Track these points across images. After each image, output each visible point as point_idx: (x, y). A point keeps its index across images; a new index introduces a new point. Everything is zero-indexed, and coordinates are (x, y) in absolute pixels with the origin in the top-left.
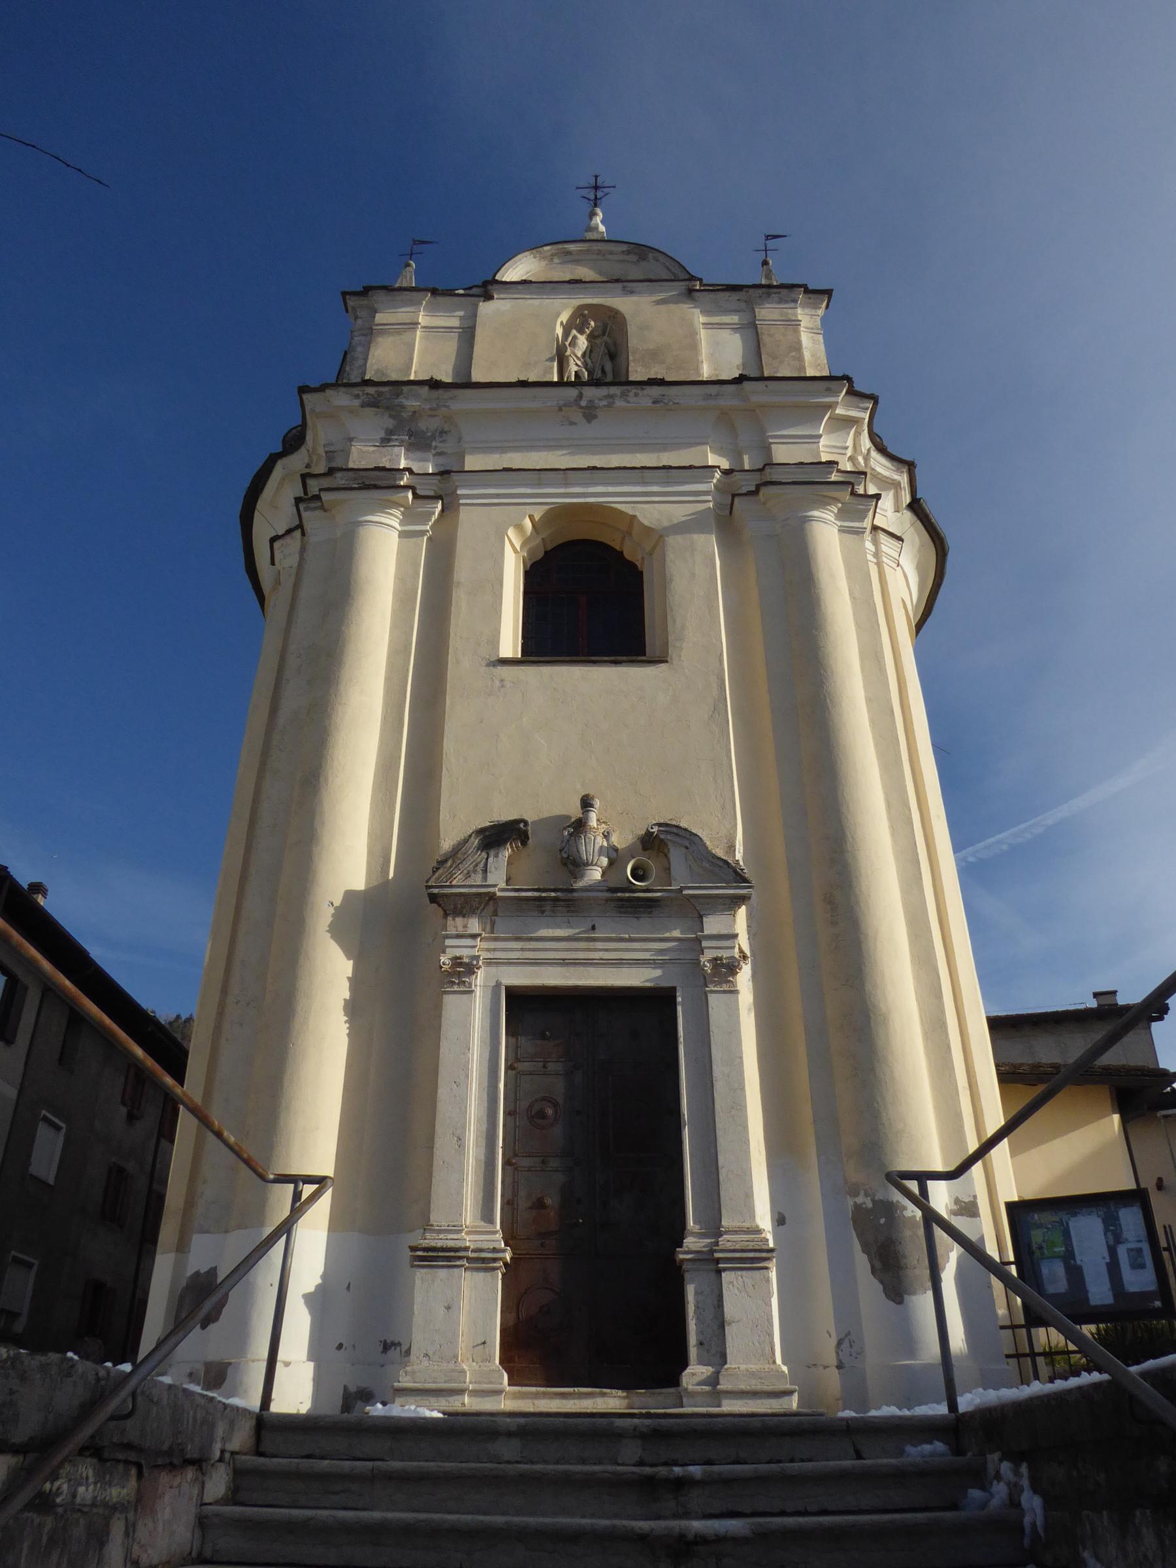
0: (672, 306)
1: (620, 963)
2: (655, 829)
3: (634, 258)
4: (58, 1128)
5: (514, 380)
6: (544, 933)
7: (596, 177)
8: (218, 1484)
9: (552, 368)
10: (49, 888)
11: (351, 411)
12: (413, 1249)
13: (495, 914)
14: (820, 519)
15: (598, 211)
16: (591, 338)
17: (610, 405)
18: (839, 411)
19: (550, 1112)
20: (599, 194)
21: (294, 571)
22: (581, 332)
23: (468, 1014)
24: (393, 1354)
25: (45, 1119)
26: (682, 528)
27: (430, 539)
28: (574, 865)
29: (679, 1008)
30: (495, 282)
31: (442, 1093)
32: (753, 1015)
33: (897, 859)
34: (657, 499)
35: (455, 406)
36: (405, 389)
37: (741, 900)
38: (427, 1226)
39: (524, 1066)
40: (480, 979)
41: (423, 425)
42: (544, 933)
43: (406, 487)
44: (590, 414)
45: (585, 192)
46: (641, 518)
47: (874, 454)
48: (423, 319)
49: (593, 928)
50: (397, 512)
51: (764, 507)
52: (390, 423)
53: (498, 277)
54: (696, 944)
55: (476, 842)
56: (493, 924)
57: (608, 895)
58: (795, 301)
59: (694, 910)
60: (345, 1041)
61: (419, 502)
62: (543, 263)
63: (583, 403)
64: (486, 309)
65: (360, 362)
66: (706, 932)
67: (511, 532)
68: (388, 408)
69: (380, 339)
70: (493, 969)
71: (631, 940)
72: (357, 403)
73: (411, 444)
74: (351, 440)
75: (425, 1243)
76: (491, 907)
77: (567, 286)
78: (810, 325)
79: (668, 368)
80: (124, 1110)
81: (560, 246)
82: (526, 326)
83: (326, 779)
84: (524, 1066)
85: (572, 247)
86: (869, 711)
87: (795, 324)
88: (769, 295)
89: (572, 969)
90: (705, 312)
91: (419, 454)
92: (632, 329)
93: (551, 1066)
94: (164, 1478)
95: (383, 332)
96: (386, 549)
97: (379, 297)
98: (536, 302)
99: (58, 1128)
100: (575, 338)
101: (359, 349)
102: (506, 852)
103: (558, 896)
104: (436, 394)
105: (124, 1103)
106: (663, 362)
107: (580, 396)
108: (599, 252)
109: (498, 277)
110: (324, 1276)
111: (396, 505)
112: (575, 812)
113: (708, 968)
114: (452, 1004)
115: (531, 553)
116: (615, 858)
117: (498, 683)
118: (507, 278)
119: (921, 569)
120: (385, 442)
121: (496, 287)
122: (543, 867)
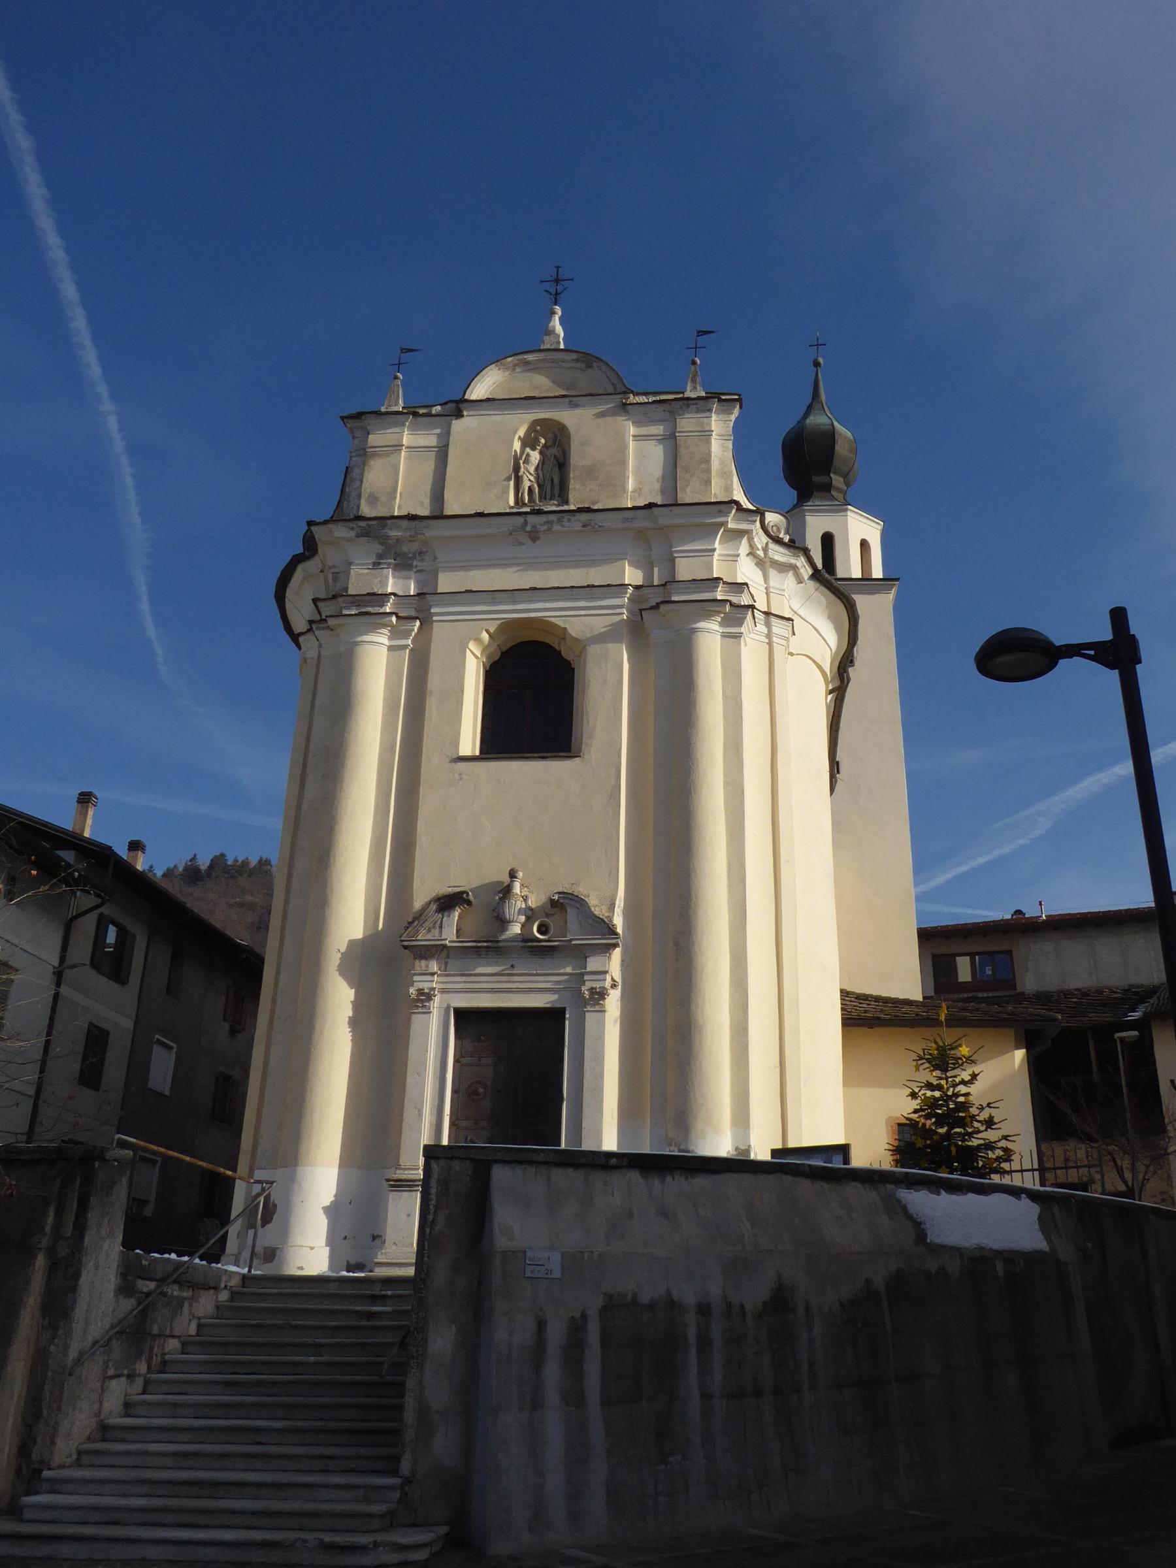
0: (609, 419)
1: (528, 991)
2: (556, 897)
3: (580, 365)
4: (170, 1048)
5: (473, 512)
6: (480, 970)
7: (558, 268)
8: (224, 1296)
9: (508, 487)
10: (146, 843)
11: (349, 540)
12: (388, 1180)
13: (448, 956)
14: (708, 631)
15: (558, 309)
16: (541, 453)
17: (549, 529)
18: (730, 526)
19: (481, 1090)
20: (560, 288)
21: (315, 662)
22: (533, 449)
23: (427, 1028)
24: (378, 1241)
25: (159, 1042)
26: (602, 638)
27: (411, 650)
28: (503, 922)
29: (567, 1022)
30: (463, 401)
31: (409, 1080)
32: (618, 1025)
33: (730, 909)
34: (583, 612)
35: (429, 533)
36: (389, 522)
37: (615, 946)
38: (398, 1166)
39: (464, 1060)
40: (436, 1004)
41: (405, 548)
42: (480, 970)
43: (391, 614)
44: (534, 536)
45: (546, 286)
46: (570, 631)
47: (772, 546)
48: (406, 439)
49: (512, 966)
50: (385, 631)
51: (666, 619)
52: (379, 548)
53: (466, 397)
54: (580, 978)
55: (434, 907)
56: (446, 964)
57: (521, 944)
58: (710, 410)
59: (581, 953)
60: (350, 1044)
61: (403, 622)
62: (507, 373)
63: (528, 528)
64: (458, 426)
65: (357, 484)
66: (588, 969)
67: (472, 645)
68: (376, 538)
69: (372, 462)
70: (445, 995)
71: (537, 975)
72: (352, 534)
73: (396, 565)
74: (350, 564)
75: (395, 1177)
76: (445, 953)
77: (525, 402)
78: (723, 432)
79: (601, 485)
80: (227, 1026)
81: (521, 357)
82: (486, 453)
83: (334, 858)
84: (464, 1060)
85: (530, 357)
86: (725, 793)
87: (706, 434)
88: (688, 406)
89: (497, 995)
90: (637, 424)
91: (404, 573)
92: (574, 446)
93: (484, 1061)
94: (202, 1292)
95: (375, 455)
96: (377, 661)
97: (371, 421)
98: (498, 418)
99: (170, 1048)
100: (528, 455)
101: (357, 470)
102: (456, 914)
103: (488, 946)
104: (413, 524)
105: (225, 1020)
106: (597, 479)
107: (526, 523)
108: (554, 361)
109: (466, 397)
110: (336, 1196)
111: (384, 626)
112: (506, 879)
113: (587, 995)
114: (417, 1020)
115: (488, 657)
116: (530, 915)
117: (457, 776)
118: (474, 397)
119: (833, 619)
120: (376, 565)
121: (466, 404)
122: (481, 923)
